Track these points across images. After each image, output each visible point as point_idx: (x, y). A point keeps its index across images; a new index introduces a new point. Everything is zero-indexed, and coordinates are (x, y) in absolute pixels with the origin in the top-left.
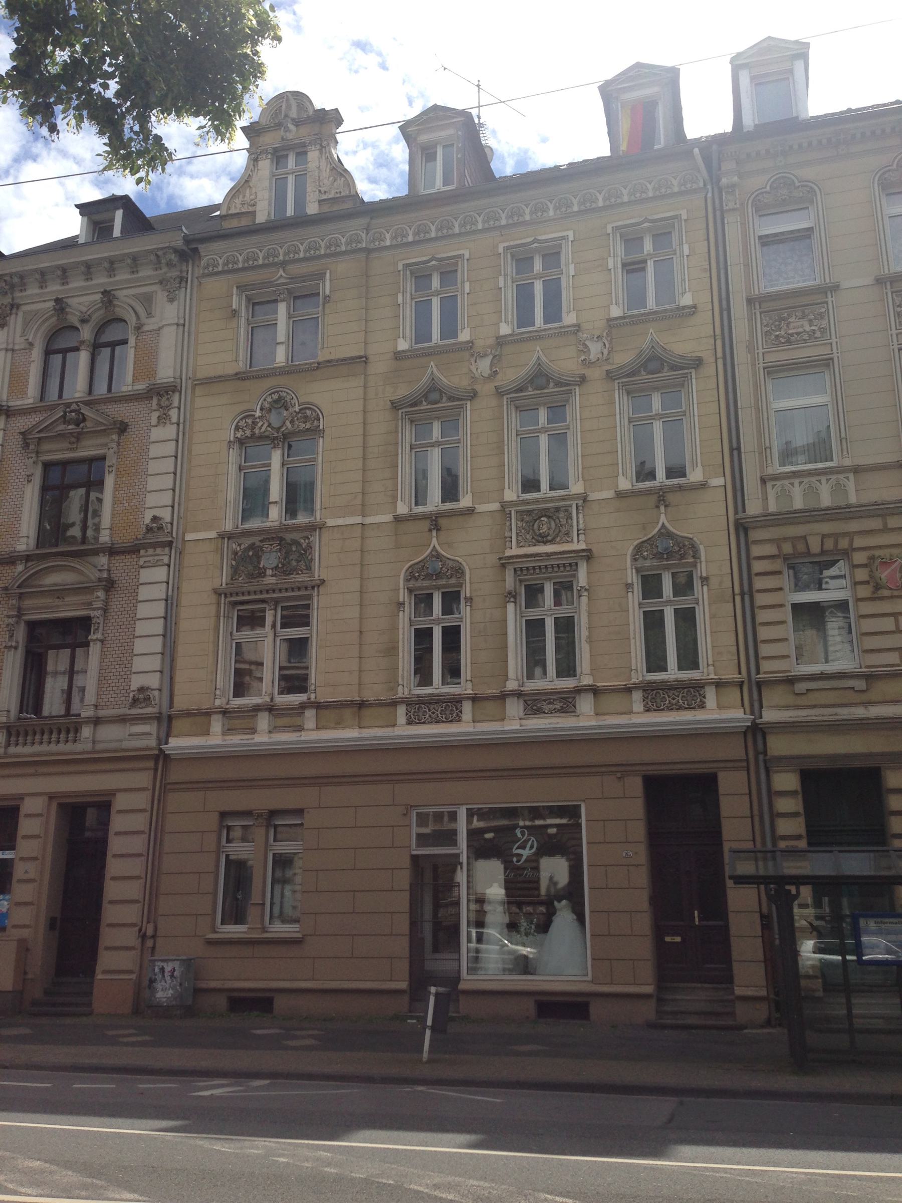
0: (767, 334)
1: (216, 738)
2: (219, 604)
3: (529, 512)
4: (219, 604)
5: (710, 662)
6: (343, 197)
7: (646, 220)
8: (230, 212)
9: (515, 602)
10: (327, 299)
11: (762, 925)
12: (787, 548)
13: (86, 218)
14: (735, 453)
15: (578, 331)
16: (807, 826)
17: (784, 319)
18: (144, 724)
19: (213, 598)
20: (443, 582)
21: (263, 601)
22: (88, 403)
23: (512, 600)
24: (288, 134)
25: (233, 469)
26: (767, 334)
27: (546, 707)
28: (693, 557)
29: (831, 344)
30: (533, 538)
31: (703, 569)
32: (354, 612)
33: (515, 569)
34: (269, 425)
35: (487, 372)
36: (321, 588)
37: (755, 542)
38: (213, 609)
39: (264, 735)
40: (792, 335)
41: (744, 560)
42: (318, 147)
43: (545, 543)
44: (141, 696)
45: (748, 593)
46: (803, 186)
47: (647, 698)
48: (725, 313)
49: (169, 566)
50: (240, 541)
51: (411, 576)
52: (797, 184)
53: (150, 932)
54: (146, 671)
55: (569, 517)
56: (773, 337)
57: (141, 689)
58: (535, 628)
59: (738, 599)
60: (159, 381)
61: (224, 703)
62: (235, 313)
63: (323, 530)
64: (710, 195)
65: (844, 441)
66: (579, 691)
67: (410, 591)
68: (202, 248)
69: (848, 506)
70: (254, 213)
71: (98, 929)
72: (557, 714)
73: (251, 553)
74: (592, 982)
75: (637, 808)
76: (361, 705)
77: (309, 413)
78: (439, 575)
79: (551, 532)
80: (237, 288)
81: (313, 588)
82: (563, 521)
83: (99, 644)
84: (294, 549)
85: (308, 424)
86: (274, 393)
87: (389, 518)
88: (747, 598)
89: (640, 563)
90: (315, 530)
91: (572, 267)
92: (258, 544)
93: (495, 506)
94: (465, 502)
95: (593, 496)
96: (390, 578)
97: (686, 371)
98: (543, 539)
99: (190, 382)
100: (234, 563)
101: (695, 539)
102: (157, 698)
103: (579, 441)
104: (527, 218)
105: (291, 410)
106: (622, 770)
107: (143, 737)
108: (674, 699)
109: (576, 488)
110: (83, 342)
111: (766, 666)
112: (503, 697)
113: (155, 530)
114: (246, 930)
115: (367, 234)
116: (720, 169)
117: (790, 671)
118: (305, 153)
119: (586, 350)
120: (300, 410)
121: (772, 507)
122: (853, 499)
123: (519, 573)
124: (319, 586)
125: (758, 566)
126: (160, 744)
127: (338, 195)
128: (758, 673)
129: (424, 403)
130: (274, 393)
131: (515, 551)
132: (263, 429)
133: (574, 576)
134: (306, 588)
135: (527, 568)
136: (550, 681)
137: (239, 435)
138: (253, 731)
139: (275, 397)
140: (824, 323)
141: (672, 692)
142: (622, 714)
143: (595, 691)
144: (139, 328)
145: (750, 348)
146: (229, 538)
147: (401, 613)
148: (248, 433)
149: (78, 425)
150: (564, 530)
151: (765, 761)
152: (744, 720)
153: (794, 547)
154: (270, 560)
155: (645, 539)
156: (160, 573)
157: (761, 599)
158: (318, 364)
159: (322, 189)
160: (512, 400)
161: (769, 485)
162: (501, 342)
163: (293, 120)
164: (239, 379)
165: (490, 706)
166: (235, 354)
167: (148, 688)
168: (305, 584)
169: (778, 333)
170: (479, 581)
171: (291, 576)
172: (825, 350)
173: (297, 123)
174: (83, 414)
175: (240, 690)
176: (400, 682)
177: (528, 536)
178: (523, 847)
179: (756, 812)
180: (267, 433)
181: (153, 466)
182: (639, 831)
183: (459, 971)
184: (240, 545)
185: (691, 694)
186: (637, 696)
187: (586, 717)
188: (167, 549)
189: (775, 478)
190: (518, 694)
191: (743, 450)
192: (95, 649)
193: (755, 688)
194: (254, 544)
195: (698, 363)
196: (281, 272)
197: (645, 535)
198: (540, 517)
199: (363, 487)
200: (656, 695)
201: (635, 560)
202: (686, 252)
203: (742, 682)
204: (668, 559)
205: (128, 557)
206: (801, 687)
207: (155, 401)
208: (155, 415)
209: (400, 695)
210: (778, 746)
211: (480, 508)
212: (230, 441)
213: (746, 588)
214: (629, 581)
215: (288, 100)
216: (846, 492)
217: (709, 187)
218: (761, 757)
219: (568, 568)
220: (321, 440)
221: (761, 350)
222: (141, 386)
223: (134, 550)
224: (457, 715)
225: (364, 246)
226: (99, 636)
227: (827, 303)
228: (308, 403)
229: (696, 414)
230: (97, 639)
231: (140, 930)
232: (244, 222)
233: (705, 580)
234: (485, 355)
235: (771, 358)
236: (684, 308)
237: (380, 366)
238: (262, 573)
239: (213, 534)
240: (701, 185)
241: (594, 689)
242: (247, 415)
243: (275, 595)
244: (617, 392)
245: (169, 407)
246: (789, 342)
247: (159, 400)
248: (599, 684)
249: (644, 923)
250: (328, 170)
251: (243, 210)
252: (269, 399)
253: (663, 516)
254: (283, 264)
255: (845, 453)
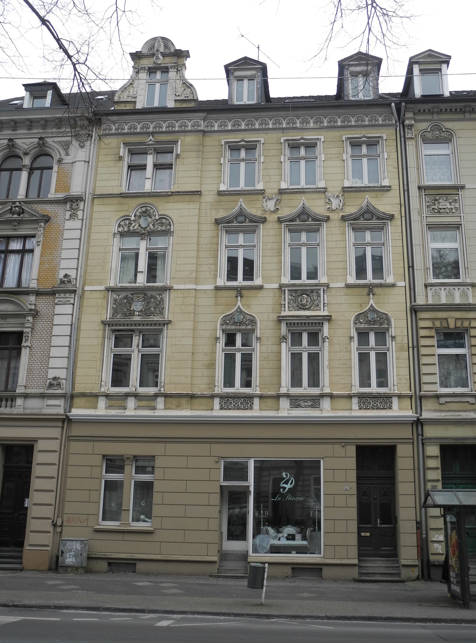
0: (428, 206)
1: (102, 410)
2: (104, 330)
3: (296, 291)
4: (104, 330)
5: (395, 384)
6: (189, 100)
7: (364, 137)
8: (120, 100)
9: (286, 342)
10: (178, 156)
11: (417, 527)
12: (438, 324)
13: (28, 93)
14: (411, 269)
15: (326, 191)
16: (442, 475)
17: (437, 200)
18: (57, 399)
19: (101, 327)
20: (243, 327)
21: (132, 330)
22: (25, 202)
23: (285, 341)
24: (158, 60)
25: (116, 249)
26: (428, 206)
27: (302, 403)
28: (387, 324)
29: (461, 217)
30: (298, 306)
31: (393, 331)
32: (189, 341)
33: (287, 323)
34: (140, 226)
35: (272, 209)
36: (169, 325)
37: (421, 319)
38: (101, 333)
39: (132, 410)
40: (441, 209)
41: (415, 329)
42: (176, 70)
43: (304, 309)
44: (55, 382)
45: (416, 347)
46: (447, 131)
47: (361, 402)
48: (406, 193)
49: (73, 305)
50: (119, 293)
51: (224, 322)
52: (444, 130)
53: (59, 523)
54: (57, 367)
55: (319, 296)
56: (431, 209)
57: (55, 379)
58: (296, 359)
59: (411, 350)
60: (72, 194)
61: (106, 390)
62: (121, 158)
63: (171, 291)
64: (398, 128)
65: (467, 269)
66: (322, 396)
67: (223, 331)
68: (104, 119)
69: (470, 304)
70: (135, 102)
71: (25, 520)
72: (309, 408)
73: (125, 301)
74: (324, 557)
75: (352, 463)
76: (192, 397)
77: (164, 221)
78: (241, 323)
79: (308, 303)
80: (123, 143)
81: (164, 325)
82: (315, 298)
83: (28, 349)
84: (152, 300)
85: (163, 227)
86: (143, 207)
87: (212, 287)
88: (415, 349)
89: (358, 326)
90: (166, 290)
91: (323, 156)
92: (130, 296)
93: (276, 286)
94: (257, 281)
95: (331, 285)
96: (211, 323)
97: (385, 221)
98: (303, 307)
99: (91, 196)
100: (114, 306)
101: (389, 314)
102: (64, 385)
103: (325, 253)
104: (298, 125)
105: (153, 218)
106: (344, 442)
107: (56, 407)
108: (375, 403)
109: (323, 279)
110: (24, 166)
111: (425, 388)
112: (278, 397)
113: (66, 282)
114: (119, 524)
115: (204, 122)
116: (404, 116)
117: (437, 391)
118: (168, 72)
119: (329, 202)
120: (159, 218)
121: (430, 302)
122: (471, 301)
123: (289, 326)
124: (167, 324)
125: (422, 333)
126: (65, 412)
127: (186, 98)
128: (420, 391)
129: (235, 222)
130: (143, 207)
131: (286, 313)
132: (136, 227)
133: (320, 330)
134: (160, 325)
135: (294, 323)
136: (305, 389)
137: (120, 230)
138: (125, 408)
139: (144, 209)
140: (457, 205)
141: (374, 399)
142: (346, 410)
143: (331, 396)
144: (60, 161)
145: (420, 213)
146: (112, 291)
147: (218, 344)
148: (126, 229)
149: (19, 215)
150: (315, 303)
151: (422, 440)
152: (414, 417)
153: (441, 323)
154: (137, 306)
155: (361, 312)
156: (68, 309)
157: (424, 351)
158: (172, 193)
159: (177, 94)
160: (287, 226)
161: (429, 288)
162: (281, 192)
163: (161, 53)
164: (122, 197)
165: (270, 402)
166: (120, 182)
167: (59, 378)
168: (159, 322)
169: (434, 207)
170: (265, 327)
171: (151, 317)
172: (457, 219)
173: (164, 55)
174: (23, 209)
175: (116, 382)
176: (216, 384)
177: (294, 305)
178: (286, 483)
179: (416, 467)
180: (138, 230)
181: (66, 244)
182: (353, 476)
183: (248, 552)
184: (119, 296)
185: (385, 400)
186: (355, 400)
187: (326, 410)
188: (73, 295)
189: (432, 285)
190: (287, 396)
191: (415, 268)
192: (25, 353)
193: (419, 399)
194: (127, 296)
195: (391, 217)
196: (151, 137)
197: (361, 310)
198: (302, 295)
199: (197, 268)
200: (366, 400)
201: (355, 323)
202: (386, 157)
203: (412, 396)
204: (373, 324)
205: (47, 297)
206: (442, 400)
207: (68, 206)
208: (68, 214)
209: (216, 392)
210: (429, 431)
211: (266, 286)
212: (115, 233)
213: (415, 344)
214: (352, 336)
215: (159, 41)
216: (467, 296)
217: (398, 124)
218: (420, 437)
219: (317, 325)
220: (172, 237)
221: (425, 215)
222: (61, 195)
223: (53, 293)
224: (250, 405)
225: (202, 128)
226: (28, 344)
227: (458, 194)
228: (164, 215)
229: (390, 245)
230: (27, 346)
231: (53, 522)
232: (129, 107)
233: (393, 338)
234: (272, 199)
235: (430, 220)
236: (384, 187)
237: (209, 197)
238: (132, 313)
239: (102, 288)
240: (394, 122)
241: (331, 396)
242: (126, 218)
243: (140, 327)
244: (347, 228)
245: (77, 209)
246: (439, 212)
247: (72, 205)
248: (334, 393)
249: (354, 526)
250: (181, 84)
251: (128, 100)
252: (140, 211)
253: (371, 300)
254: (153, 133)
255: (467, 276)
